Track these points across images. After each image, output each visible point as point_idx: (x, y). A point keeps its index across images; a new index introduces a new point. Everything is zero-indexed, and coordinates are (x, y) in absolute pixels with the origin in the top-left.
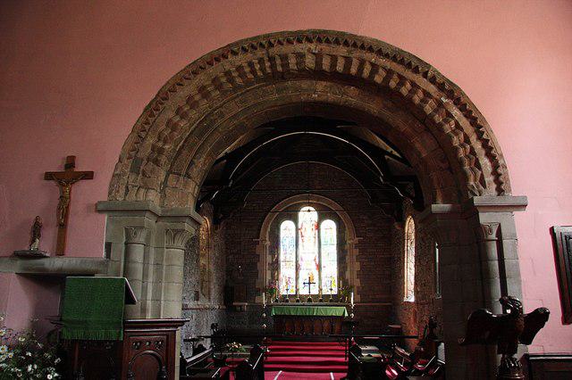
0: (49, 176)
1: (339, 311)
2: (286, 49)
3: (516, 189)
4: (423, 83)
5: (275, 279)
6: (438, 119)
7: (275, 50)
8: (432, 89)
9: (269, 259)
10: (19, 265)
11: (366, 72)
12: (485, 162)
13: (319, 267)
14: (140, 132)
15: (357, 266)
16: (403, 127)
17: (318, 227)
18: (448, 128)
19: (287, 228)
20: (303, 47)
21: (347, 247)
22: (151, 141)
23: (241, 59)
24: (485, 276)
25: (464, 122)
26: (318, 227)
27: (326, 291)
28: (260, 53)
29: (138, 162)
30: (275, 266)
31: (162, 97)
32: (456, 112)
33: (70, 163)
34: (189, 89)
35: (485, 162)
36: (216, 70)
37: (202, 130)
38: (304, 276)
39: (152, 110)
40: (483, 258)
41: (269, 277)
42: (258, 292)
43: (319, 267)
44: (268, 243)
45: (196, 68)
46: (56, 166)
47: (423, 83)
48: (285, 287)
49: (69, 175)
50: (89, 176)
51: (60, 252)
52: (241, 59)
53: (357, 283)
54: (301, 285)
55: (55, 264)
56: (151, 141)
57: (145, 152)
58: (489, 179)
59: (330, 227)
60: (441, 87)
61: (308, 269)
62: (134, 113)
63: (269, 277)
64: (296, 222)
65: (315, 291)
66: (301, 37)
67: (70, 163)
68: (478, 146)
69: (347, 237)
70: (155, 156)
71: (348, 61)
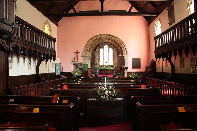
0: (75, 52)
1: (112, 68)
2: (102, 36)
3: (128, 54)
4: (119, 41)
5: (99, 62)
6: (120, 45)
7: (102, 36)
8: (120, 41)
9: (98, 57)
10: (73, 63)
11: (112, 39)
12: (125, 51)
13: (109, 59)
14: (85, 47)
15: (117, 59)
16: (117, 46)
17: (108, 50)
18: (121, 46)
19: (101, 50)
20: (104, 36)
21: (115, 55)
22: (86, 48)
23: (97, 38)
24: (124, 63)
25: (123, 46)
26: (108, 50)
27: (110, 64)
28: (99, 37)
29: (85, 50)
30: (99, 59)
31: (88, 42)
32: (122, 44)
33: (77, 51)
34: (91, 41)
35: (125, 51)
36: (94, 39)
37: (92, 46)
38: (105, 61)
39: (86, 44)
40: (124, 62)
41: (98, 61)
42: (95, 65)
43: (109, 59)
44: (97, 54)
45: (91, 39)
46: (76, 51)
47: (119, 41)
48: (101, 63)
49: (77, 52)
50: (80, 52)
51: (77, 61)
52: (97, 38)
53: (117, 63)
54: (105, 63)
55: (77, 63)
56: (86, 48)
57: (86, 49)
58: (126, 53)
59: (111, 50)
60: (121, 41)
61: (106, 60)
62: (84, 45)
63: (98, 61)
64: (103, 49)
65: (108, 64)
66: (104, 35)
67: (77, 51)
68: (125, 49)
69: (115, 52)
70: (87, 49)
71: (110, 38)
